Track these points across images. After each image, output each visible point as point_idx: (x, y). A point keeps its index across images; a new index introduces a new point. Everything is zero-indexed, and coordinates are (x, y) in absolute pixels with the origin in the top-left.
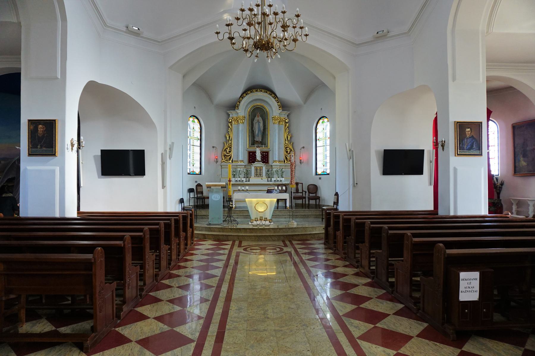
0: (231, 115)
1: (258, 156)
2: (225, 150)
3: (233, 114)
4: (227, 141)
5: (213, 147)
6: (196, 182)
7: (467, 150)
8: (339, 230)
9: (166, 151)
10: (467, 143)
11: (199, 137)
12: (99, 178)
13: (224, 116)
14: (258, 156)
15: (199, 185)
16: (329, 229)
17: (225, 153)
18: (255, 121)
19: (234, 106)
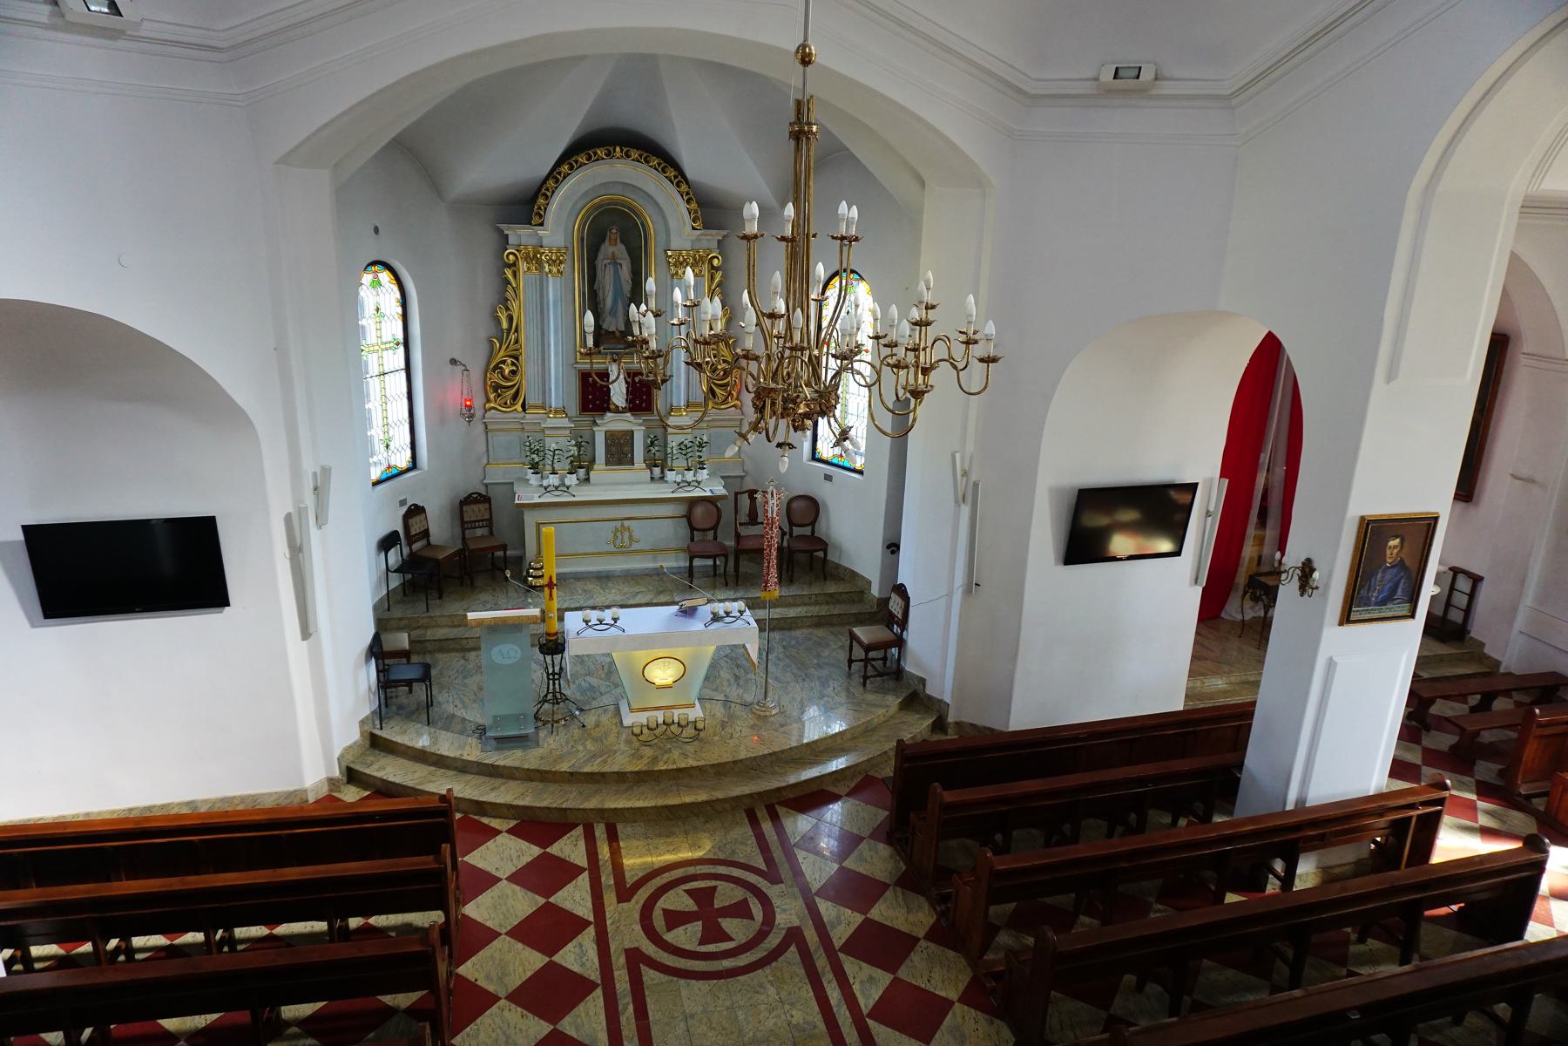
0: (512, 240)
1: (618, 393)
2: (497, 367)
3: (520, 235)
4: (501, 335)
5: (454, 362)
6: (403, 503)
7: (1377, 604)
9: (301, 512)
10: (1382, 581)
11: (400, 337)
12: (33, 625)
13: (484, 238)
14: (618, 393)
15: (415, 511)
17: (496, 378)
18: (601, 261)
19: (526, 205)
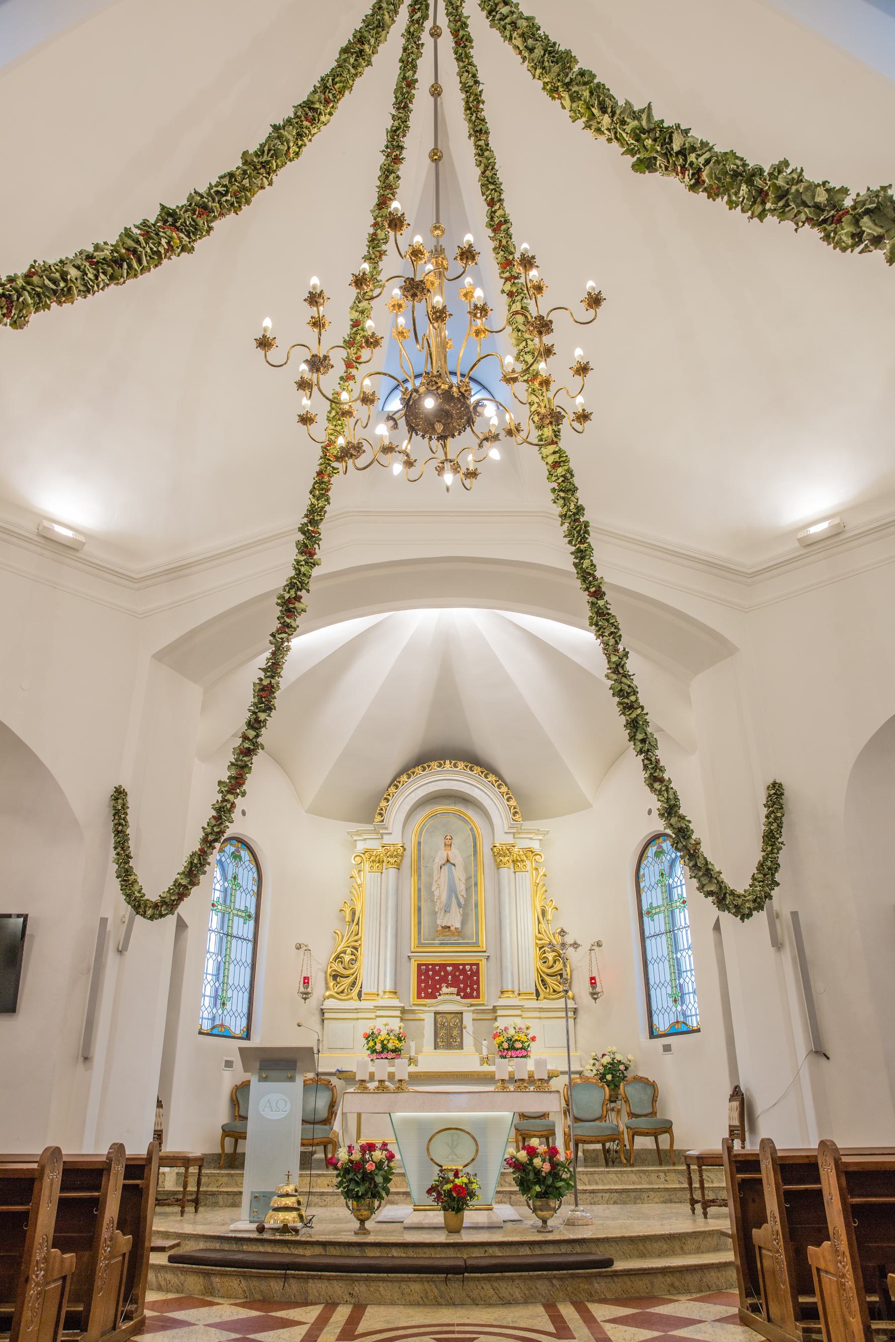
2: (338, 957)
8: (821, 1234)
11: (253, 911)
16: (758, 1235)
